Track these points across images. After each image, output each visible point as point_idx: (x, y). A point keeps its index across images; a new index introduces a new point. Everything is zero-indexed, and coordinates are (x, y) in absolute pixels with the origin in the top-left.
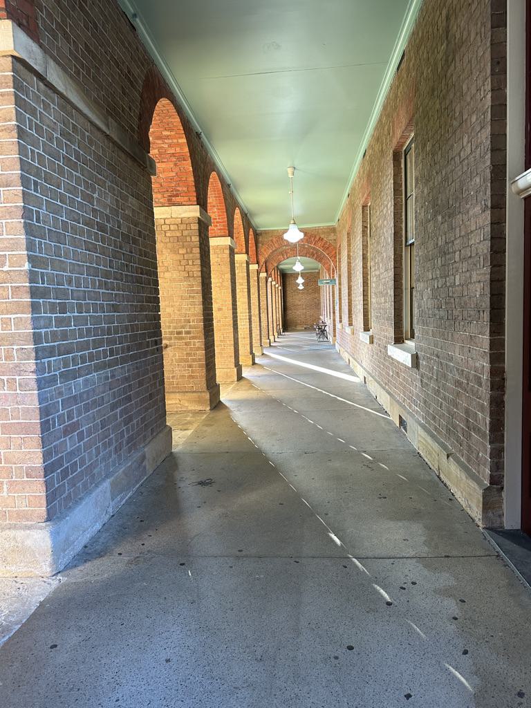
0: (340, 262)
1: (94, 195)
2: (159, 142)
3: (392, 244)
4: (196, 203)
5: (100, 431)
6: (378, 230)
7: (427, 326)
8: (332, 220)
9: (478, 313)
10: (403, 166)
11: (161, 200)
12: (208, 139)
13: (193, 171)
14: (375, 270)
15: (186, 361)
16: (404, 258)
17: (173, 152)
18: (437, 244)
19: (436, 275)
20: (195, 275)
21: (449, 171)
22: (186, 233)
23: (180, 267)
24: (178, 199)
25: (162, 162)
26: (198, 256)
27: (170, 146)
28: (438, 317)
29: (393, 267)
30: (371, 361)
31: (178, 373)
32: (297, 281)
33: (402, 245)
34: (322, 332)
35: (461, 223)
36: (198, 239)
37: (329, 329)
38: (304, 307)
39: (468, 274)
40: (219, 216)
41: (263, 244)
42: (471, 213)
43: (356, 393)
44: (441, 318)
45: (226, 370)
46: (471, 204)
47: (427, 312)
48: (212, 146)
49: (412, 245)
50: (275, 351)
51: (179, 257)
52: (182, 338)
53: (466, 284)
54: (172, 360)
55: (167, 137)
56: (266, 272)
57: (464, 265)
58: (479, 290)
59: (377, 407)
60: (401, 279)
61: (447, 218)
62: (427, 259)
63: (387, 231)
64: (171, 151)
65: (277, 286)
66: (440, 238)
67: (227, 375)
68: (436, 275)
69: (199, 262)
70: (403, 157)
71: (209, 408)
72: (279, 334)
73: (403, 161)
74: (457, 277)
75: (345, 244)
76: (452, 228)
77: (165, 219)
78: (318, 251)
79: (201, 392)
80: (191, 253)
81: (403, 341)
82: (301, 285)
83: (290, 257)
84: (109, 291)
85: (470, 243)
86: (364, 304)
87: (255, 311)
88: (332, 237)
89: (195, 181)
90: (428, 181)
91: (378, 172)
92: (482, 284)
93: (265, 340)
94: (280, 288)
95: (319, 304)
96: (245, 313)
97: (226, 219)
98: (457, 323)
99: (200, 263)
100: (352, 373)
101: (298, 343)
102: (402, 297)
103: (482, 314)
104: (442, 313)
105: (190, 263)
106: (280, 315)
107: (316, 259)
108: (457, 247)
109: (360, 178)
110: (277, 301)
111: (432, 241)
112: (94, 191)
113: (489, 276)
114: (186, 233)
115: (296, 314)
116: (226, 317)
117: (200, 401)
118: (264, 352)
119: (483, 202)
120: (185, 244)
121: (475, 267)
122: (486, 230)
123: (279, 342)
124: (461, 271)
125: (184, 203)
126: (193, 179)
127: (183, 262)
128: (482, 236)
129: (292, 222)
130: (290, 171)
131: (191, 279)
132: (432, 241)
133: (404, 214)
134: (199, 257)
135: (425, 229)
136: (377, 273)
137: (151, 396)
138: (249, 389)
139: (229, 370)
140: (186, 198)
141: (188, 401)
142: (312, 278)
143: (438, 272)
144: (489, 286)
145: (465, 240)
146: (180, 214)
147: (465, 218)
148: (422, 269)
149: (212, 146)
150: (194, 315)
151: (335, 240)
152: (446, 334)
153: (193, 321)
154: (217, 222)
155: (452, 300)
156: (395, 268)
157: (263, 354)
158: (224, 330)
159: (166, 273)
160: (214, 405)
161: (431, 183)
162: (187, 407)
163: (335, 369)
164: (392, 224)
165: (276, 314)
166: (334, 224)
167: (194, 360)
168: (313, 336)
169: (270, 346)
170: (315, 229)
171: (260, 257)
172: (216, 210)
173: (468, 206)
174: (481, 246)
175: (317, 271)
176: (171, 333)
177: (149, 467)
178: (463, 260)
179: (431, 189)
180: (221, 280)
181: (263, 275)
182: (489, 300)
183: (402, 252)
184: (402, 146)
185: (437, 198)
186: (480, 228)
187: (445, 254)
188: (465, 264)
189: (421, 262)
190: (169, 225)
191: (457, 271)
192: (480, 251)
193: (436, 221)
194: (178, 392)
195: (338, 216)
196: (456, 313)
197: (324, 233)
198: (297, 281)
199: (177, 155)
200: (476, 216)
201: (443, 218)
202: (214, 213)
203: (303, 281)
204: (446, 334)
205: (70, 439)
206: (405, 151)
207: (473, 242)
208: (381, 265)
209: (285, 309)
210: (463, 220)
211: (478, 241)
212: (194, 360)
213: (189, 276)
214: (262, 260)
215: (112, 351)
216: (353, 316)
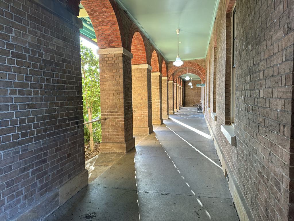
0: (206, 76)
1: (11, 35)
2: (102, 15)
3: (225, 67)
4: (121, 46)
5: (6, 189)
6: (219, 59)
7: (241, 121)
8: (204, 56)
9: (278, 126)
10: (232, 21)
11: (105, 45)
12: (132, 14)
13: (120, 30)
14: (218, 81)
15: (115, 127)
16: (231, 75)
17: (109, 20)
18: (248, 66)
19: (247, 87)
20: (120, 83)
21: (257, 10)
22: (116, 62)
23: (113, 79)
24: (113, 44)
25: (104, 25)
26: (122, 73)
27: (107, 17)
28: (247, 117)
29: (225, 80)
30: (216, 129)
31: (111, 133)
32: (189, 84)
33: (230, 67)
34: (200, 107)
35: (265, 48)
36: (122, 65)
37: (203, 107)
38: (193, 96)
39: (270, 90)
40: (142, 54)
41: (170, 68)
42: (274, 38)
43: (207, 146)
44: (250, 119)
45: (144, 128)
46: (274, 31)
47: (241, 112)
48: (135, 19)
49: (234, 68)
50: (175, 117)
51: (112, 74)
52: (113, 115)
53: (269, 98)
54: (108, 126)
55: (105, 12)
56: (173, 80)
57: (267, 82)
58: (280, 106)
59: (215, 158)
60: (230, 87)
61: (255, 46)
62: (242, 76)
63: (223, 59)
64: (108, 19)
65: (180, 86)
66: (250, 62)
67: (144, 131)
68: (247, 87)
69: (122, 76)
70: (232, 15)
71: (125, 152)
72: (180, 108)
73: (232, 18)
74: (261, 91)
75: (208, 67)
76: (258, 53)
77: (106, 55)
78: (197, 71)
79: (122, 143)
80: (119, 72)
81: (231, 124)
82: (192, 86)
83: (184, 74)
84: (25, 96)
85: (273, 64)
86: (214, 98)
87: (164, 97)
88: (203, 64)
89: (121, 35)
90: (243, 23)
91: (220, 27)
92: (283, 101)
93: (171, 111)
94: (182, 87)
95: (200, 94)
96: (158, 100)
97: (146, 56)
98: (260, 128)
99: (123, 77)
100: (208, 133)
101: (187, 113)
102: (230, 98)
103: (282, 127)
104: (250, 116)
105: (118, 77)
106: (182, 100)
107: (197, 74)
108: (261, 68)
109: (213, 33)
110: (180, 93)
111: (245, 64)
112: (11, 31)
113: (291, 95)
114: (116, 62)
115: (190, 98)
116: (145, 103)
117: (121, 148)
118: (170, 117)
119: (286, 26)
120: (116, 67)
121: (276, 85)
122: (288, 51)
123: (179, 112)
124: (264, 87)
125: (116, 46)
126: (120, 34)
127: (115, 77)
128: (284, 57)
129: (178, 56)
130: (177, 31)
131: (118, 85)
132: (245, 64)
133: (232, 49)
134: (122, 74)
135: (241, 56)
136: (219, 83)
137: (69, 155)
138: (153, 139)
139: (145, 128)
140: (117, 44)
141: (115, 147)
142: (195, 82)
143: (248, 86)
144: (290, 104)
145: (269, 61)
146: (113, 52)
147: (269, 43)
148: (239, 82)
149: (135, 19)
150: (119, 103)
151: (205, 65)
152: (252, 132)
153: (119, 107)
154: (141, 57)
155: (257, 108)
156: (226, 80)
157: (169, 118)
158: (144, 109)
159: (106, 82)
160: (129, 150)
161: (245, 24)
162: (115, 150)
163: (136, 177)
164: (225, 55)
165: (179, 98)
166: (205, 58)
167: (119, 127)
168: (195, 110)
169: (174, 114)
170: (195, 60)
171: (169, 74)
172: (141, 51)
173: (272, 33)
174: (283, 66)
175: (200, 80)
176: (108, 112)
177: (62, 200)
178: (266, 78)
179: (245, 29)
180: (143, 85)
181: (171, 82)
182: (290, 117)
183: (231, 71)
184: (231, 8)
185: (249, 33)
186: (282, 50)
187: (253, 73)
188: (268, 82)
189: (239, 78)
190: (108, 58)
191: (261, 86)
192: (282, 71)
193: (247, 50)
194: (111, 143)
195: (206, 54)
196: (260, 119)
197: (199, 62)
198: (189, 84)
199: (111, 21)
200: (279, 40)
201: (252, 46)
202: (140, 52)
203: (192, 84)
204: (252, 132)
205: (29, 177)
206: (233, 12)
207: (275, 63)
208: (220, 78)
209: (184, 96)
210: (266, 46)
211: (280, 62)
212: (119, 127)
213: (117, 84)
214: (169, 75)
215: (24, 135)
216: (210, 103)
